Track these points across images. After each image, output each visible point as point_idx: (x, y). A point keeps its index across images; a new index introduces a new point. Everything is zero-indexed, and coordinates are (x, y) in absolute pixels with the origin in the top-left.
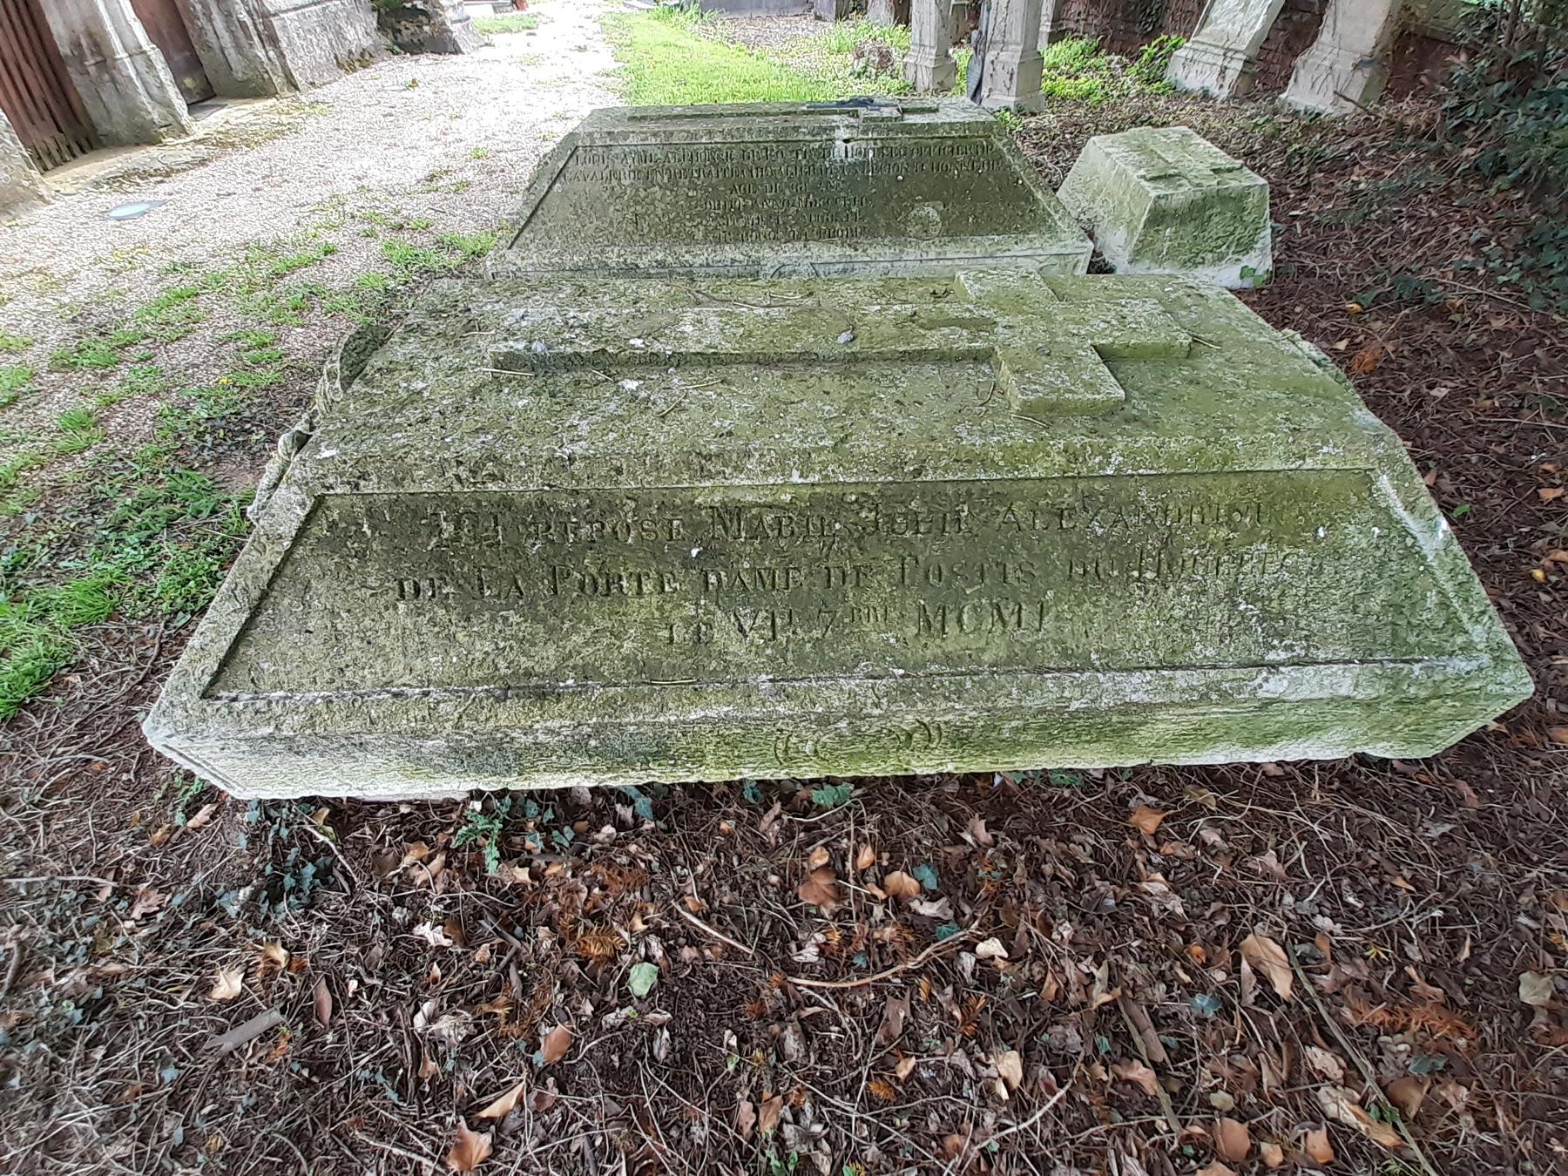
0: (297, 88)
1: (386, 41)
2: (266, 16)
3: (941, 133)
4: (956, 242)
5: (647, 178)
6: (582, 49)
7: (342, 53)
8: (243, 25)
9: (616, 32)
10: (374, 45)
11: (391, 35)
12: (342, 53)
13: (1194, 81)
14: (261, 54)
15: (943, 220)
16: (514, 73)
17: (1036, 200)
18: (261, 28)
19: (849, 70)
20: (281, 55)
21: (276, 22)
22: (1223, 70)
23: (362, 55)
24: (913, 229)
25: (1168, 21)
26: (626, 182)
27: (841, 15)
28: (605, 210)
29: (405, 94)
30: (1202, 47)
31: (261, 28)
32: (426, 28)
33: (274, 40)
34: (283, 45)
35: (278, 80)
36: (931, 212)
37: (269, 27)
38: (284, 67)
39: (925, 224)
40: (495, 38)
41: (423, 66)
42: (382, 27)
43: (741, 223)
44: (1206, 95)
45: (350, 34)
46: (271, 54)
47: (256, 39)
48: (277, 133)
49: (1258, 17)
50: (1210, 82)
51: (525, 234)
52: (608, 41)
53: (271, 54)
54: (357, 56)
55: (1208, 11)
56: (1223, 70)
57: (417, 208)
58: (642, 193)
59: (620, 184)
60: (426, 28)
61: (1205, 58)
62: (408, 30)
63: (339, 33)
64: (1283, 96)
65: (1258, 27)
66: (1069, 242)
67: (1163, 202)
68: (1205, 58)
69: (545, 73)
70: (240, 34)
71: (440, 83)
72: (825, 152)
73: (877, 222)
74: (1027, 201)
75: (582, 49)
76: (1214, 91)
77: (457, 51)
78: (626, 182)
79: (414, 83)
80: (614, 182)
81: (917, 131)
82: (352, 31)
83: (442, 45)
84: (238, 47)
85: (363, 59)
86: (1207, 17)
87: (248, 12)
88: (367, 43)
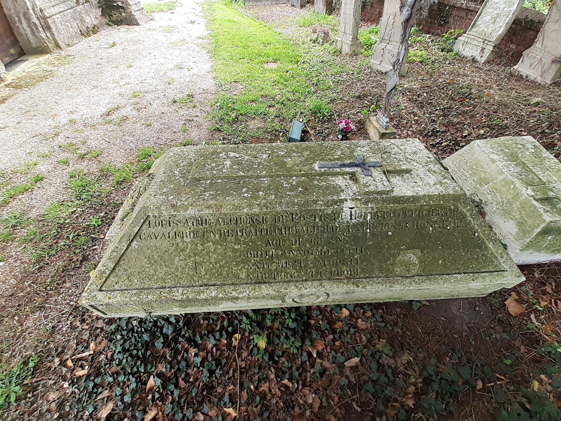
0: (60, 48)
1: (106, 20)
2: (45, 18)
3: (423, 202)
4: (429, 279)
5: (203, 236)
6: (193, 23)
7: (84, 29)
8: (35, 24)
9: (208, 10)
10: (100, 23)
11: (108, 17)
12: (84, 29)
13: (468, 52)
14: (43, 35)
15: (420, 262)
16: (161, 37)
17: (486, 248)
18: (43, 24)
19: (309, 38)
20: (53, 35)
21: (50, 21)
22: (483, 49)
23: (93, 28)
24: (398, 270)
25: (451, 20)
26: (188, 240)
27: (302, 6)
28: (172, 260)
29: (109, 50)
30: (472, 37)
31: (43, 24)
32: (123, 14)
33: (49, 28)
34: (54, 30)
35: (51, 46)
36: (412, 257)
37: (47, 23)
38: (54, 40)
39: (407, 265)
40: (156, 16)
41: (119, 33)
42: (103, 14)
43: (274, 267)
44: (474, 61)
45: (88, 19)
46: (48, 34)
47: (41, 29)
48: (44, 77)
49: (501, 27)
50: (476, 54)
51: (111, 278)
52: (205, 17)
53: (48, 34)
54: (91, 29)
55: (476, 21)
56: (483, 49)
57: (95, 140)
58: (200, 248)
59: (183, 242)
60: (123, 14)
61: (473, 43)
62: (115, 15)
63: (82, 21)
64: (516, 67)
65: (500, 32)
66: (510, 278)
67: (552, 224)
68: (473, 43)
69: (175, 37)
70: (34, 27)
71: (126, 44)
72: (336, 215)
73: (372, 264)
74: (480, 248)
75: (193, 23)
76: (478, 58)
77: (138, 24)
78: (188, 240)
79: (114, 44)
80: (179, 240)
81: (404, 202)
82: (89, 18)
83: (131, 21)
84: (33, 33)
85: (95, 30)
86: (474, 24)
87: (37, 18)
88: (96, 22)
